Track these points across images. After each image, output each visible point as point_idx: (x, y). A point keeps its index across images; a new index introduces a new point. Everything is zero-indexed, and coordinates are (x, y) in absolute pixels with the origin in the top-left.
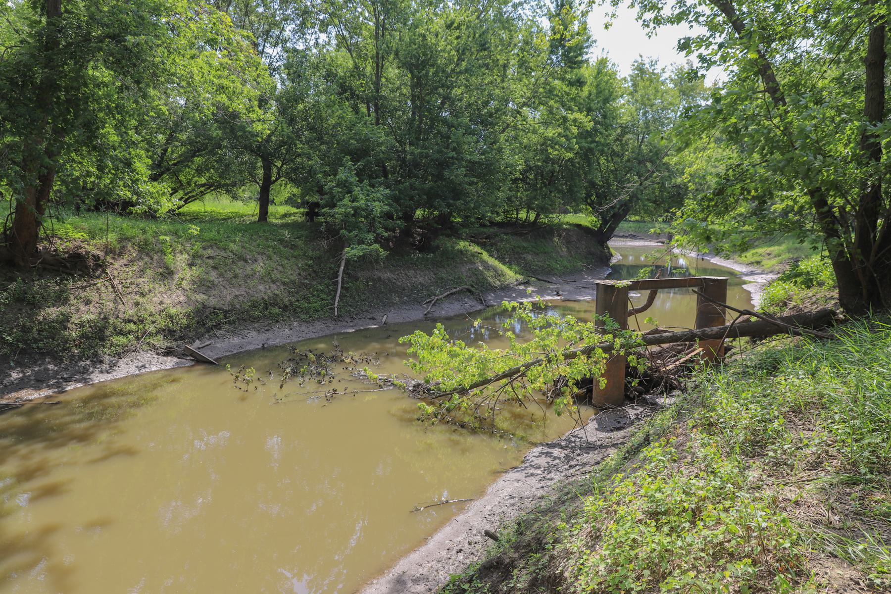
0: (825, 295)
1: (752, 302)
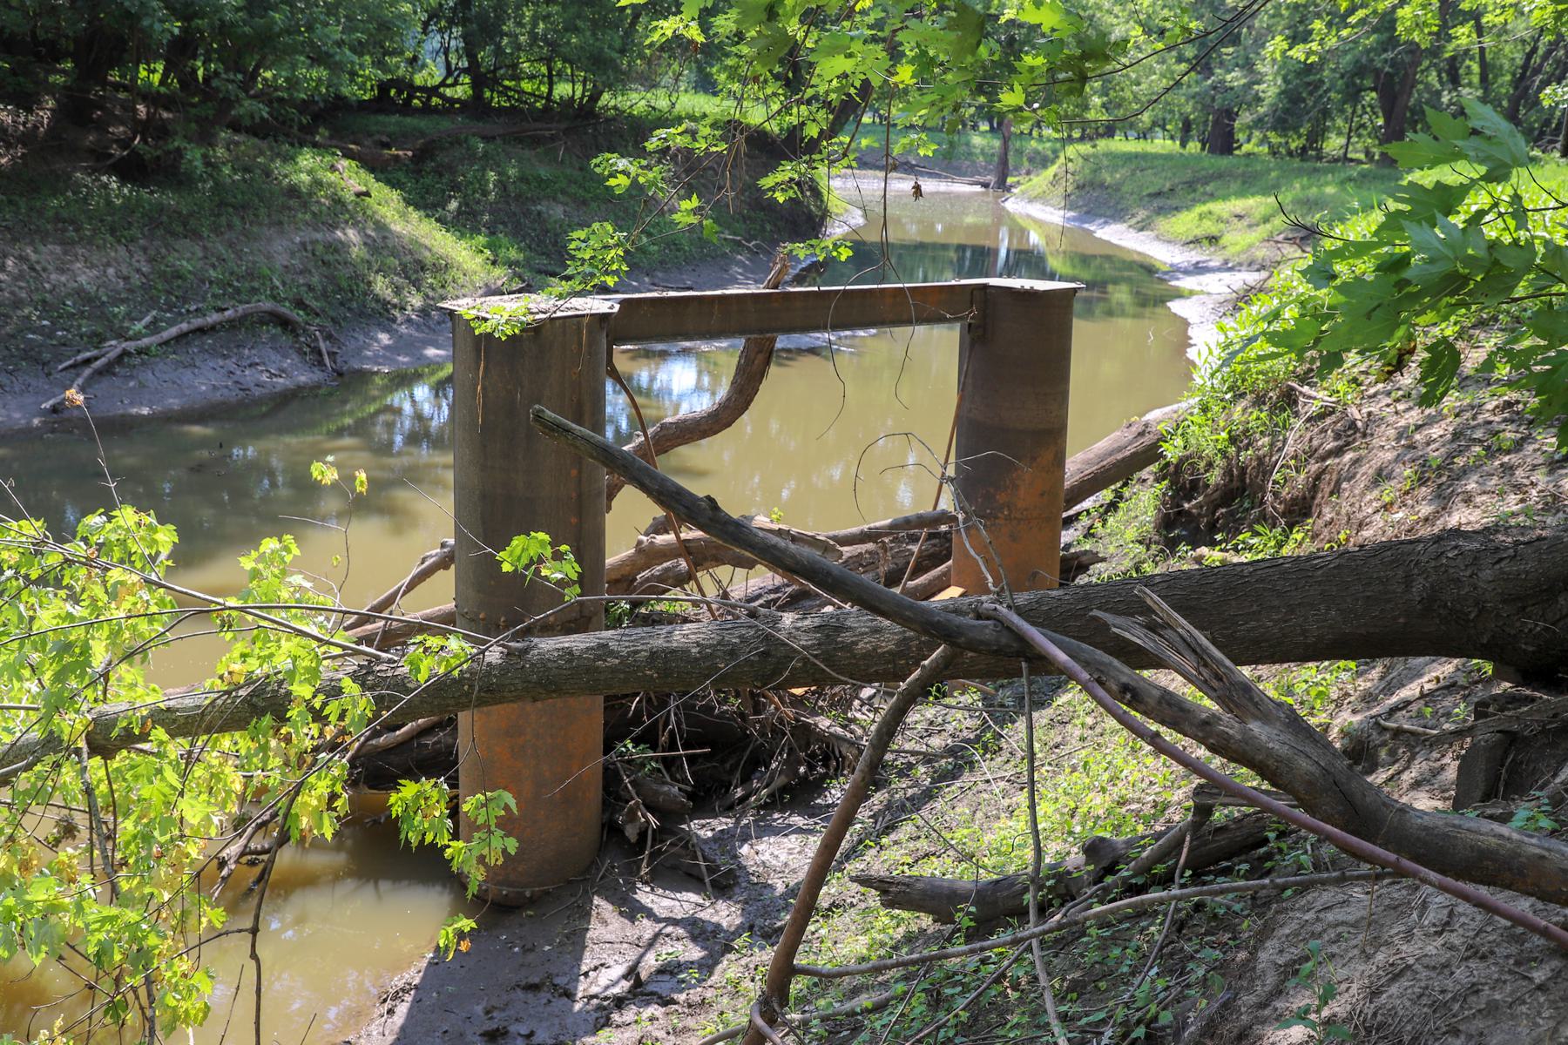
1: (1191, 353)
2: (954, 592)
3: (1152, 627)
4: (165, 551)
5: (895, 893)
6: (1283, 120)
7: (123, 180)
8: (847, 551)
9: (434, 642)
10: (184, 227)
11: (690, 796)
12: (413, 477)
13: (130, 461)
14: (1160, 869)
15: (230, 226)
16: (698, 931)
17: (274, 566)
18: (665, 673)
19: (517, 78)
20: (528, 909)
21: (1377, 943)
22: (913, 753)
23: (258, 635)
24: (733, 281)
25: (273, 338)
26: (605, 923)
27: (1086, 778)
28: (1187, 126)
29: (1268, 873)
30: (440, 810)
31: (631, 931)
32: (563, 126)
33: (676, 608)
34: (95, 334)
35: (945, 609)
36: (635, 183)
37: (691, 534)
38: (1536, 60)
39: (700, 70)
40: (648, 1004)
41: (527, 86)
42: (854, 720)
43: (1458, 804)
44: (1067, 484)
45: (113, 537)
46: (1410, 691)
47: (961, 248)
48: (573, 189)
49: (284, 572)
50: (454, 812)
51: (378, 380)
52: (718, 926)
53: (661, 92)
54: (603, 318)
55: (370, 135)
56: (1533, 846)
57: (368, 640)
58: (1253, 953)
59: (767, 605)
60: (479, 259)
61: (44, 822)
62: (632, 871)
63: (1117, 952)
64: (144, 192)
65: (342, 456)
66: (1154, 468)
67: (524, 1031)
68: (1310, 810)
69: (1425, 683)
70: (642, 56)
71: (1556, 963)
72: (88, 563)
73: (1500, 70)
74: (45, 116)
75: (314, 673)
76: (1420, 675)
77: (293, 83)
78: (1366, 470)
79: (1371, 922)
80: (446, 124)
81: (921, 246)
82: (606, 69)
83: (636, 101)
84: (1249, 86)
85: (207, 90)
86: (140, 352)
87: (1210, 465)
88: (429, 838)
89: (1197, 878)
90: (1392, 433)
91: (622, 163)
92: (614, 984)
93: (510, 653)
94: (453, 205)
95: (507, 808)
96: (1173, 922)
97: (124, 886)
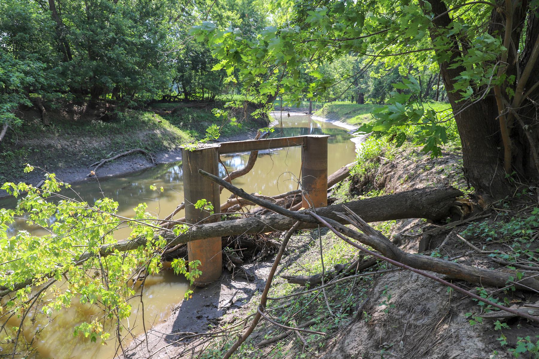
0: (444, 173)
2: (302, 209)
3: (346, 214)
4: (116, 208)
5: (291, 280)
6: (375, 96)
7: (104, 121)
8: (277, 200)
9: (180, 226)
10: (118, 132)
11: (243, 259)
12: (175, 188)
13: (108, 187)
14: (352, 271)
15: (129, 131)
16: (246, 291)
17: (142, 209)
18: (235, 231)
19: (195, 93)
20: (206, 288)
21: (401, 285)
22: (295, 247)
23: (139, 226)
24: (248, 138)
25: (140, 157)
26: (224, 290)
27: (335, 251)
28: (353, 98)
29: (377, 270)
30: (183, 265)
31: (230, 292)
32: (206, 104)
33: (237, 216)
34: (98, 158)
35: (300, 213)
36: (221, 115)
37: (239, 198)
38: (432, 79)
39: (238, 89)
40: (235, 308)
41: (198, 95)
42: (280, 240)
43: (419, 252)
44: (328, 182)
45: (103, 205)
46: (408, 227)
47: (302, 128)
48: (210, 118)
49: (144, 211)
50: (187, 266)
51: (166, 166)
52: (251, 289)
53: (229, 95)
54: (217, 148)
55: (161, 108)
56: (436, 260)
57: (165, 227)
58: (373, 289)
59: (259, 214)
60: (188, 136)
61: (92, 273)
62: (230, 278)
63: (343, 290)
64: (109, 124)
65: (157, 184)
66: (348, 178)
67: (206, 316)
68: (385, 255)
69: (412, 224)
70: (224, 87)
71: (442, 287)
72: (98, 211)
73: (424, 82)
74: (85, 107)
75: (152, 235)
76: (410, 223)
77: (142, 97)
78: (397, 176)
79: (399, 280)
80: (179, 105)
81: (292, 128)
82: (216, 90)
83: (223, 97)
84: (366, 88)
85: (122, 100)
86: (109, 161)
87: (361, 176)
88: (181, 272)
89: (360, 272)
90: (402, 167)
91: (219, 111)
92: (227, 304)
93: (198, 228)
94: (182, 123)
95: (199, 264)
96: (356, 283)
97: (110, 287)
